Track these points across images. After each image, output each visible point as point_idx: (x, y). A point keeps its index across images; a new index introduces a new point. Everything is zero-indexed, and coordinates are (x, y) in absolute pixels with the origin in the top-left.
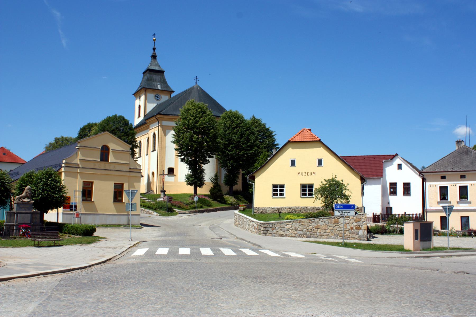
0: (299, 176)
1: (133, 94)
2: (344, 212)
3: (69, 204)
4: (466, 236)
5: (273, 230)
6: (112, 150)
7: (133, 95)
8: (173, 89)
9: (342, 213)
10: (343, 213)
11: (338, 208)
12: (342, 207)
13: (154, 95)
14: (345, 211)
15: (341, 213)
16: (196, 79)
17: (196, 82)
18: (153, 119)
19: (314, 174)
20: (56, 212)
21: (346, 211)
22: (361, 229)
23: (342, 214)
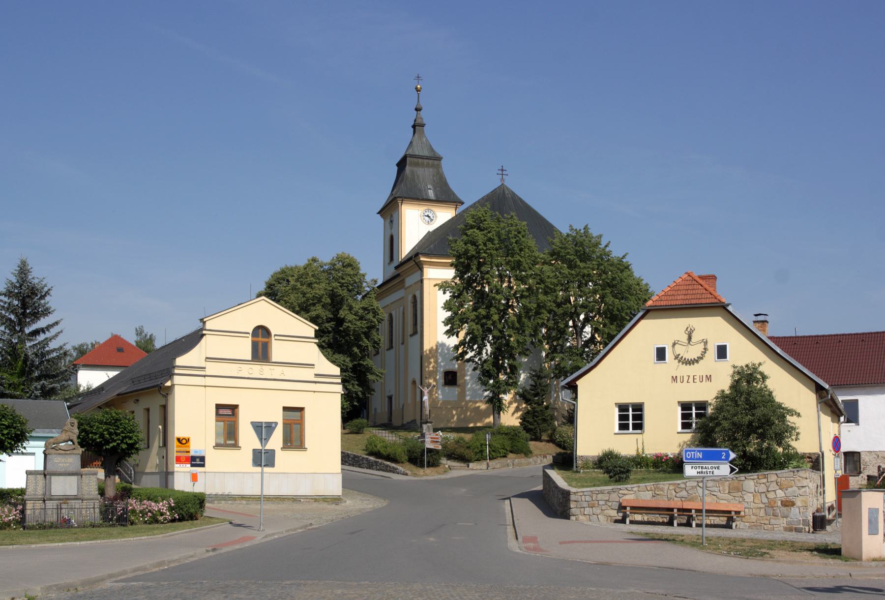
0: (675, 383)
1: (378, 211)
2: (706, 468)
3: (187, 454)
4: (749, 539)
5: (592, 507)
6: (275, 335)
7: (378, 213)
8: (462, 198)
9: (700, 470)
10: (704, 470)
11: (691, 459)
12: (701, 457)
13: (420, 212)
14: (707, 466)
15: (698, 470)
16: (500, 172)
17: (502, 179)
18: (411, 265)
19: (709, 378)
20: (260, 471)
21: (710, 466)
22: (793, 504)
23: (702, 472)
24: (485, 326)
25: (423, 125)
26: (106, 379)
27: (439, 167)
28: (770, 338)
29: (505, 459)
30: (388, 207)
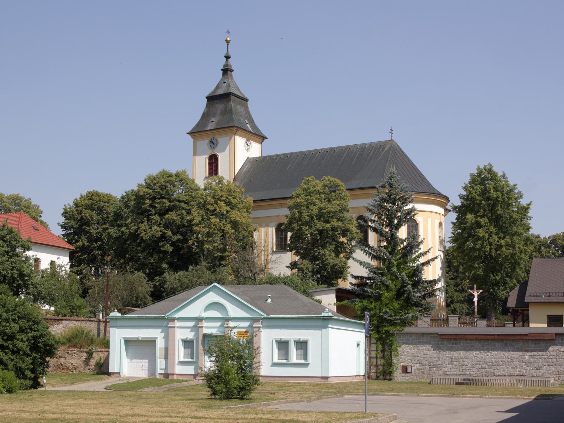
24: (203, 226)
25: (232, 71)
26: (39, 253)
27: (246, 107)
28: (136, 310)
29: (504, 328)
30: (201, 133)
